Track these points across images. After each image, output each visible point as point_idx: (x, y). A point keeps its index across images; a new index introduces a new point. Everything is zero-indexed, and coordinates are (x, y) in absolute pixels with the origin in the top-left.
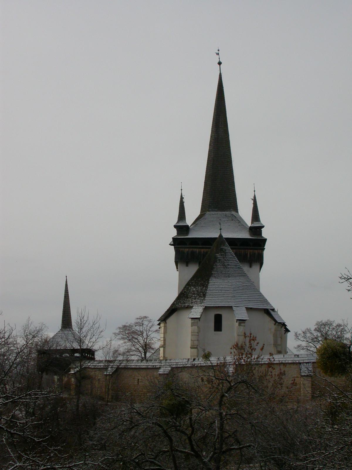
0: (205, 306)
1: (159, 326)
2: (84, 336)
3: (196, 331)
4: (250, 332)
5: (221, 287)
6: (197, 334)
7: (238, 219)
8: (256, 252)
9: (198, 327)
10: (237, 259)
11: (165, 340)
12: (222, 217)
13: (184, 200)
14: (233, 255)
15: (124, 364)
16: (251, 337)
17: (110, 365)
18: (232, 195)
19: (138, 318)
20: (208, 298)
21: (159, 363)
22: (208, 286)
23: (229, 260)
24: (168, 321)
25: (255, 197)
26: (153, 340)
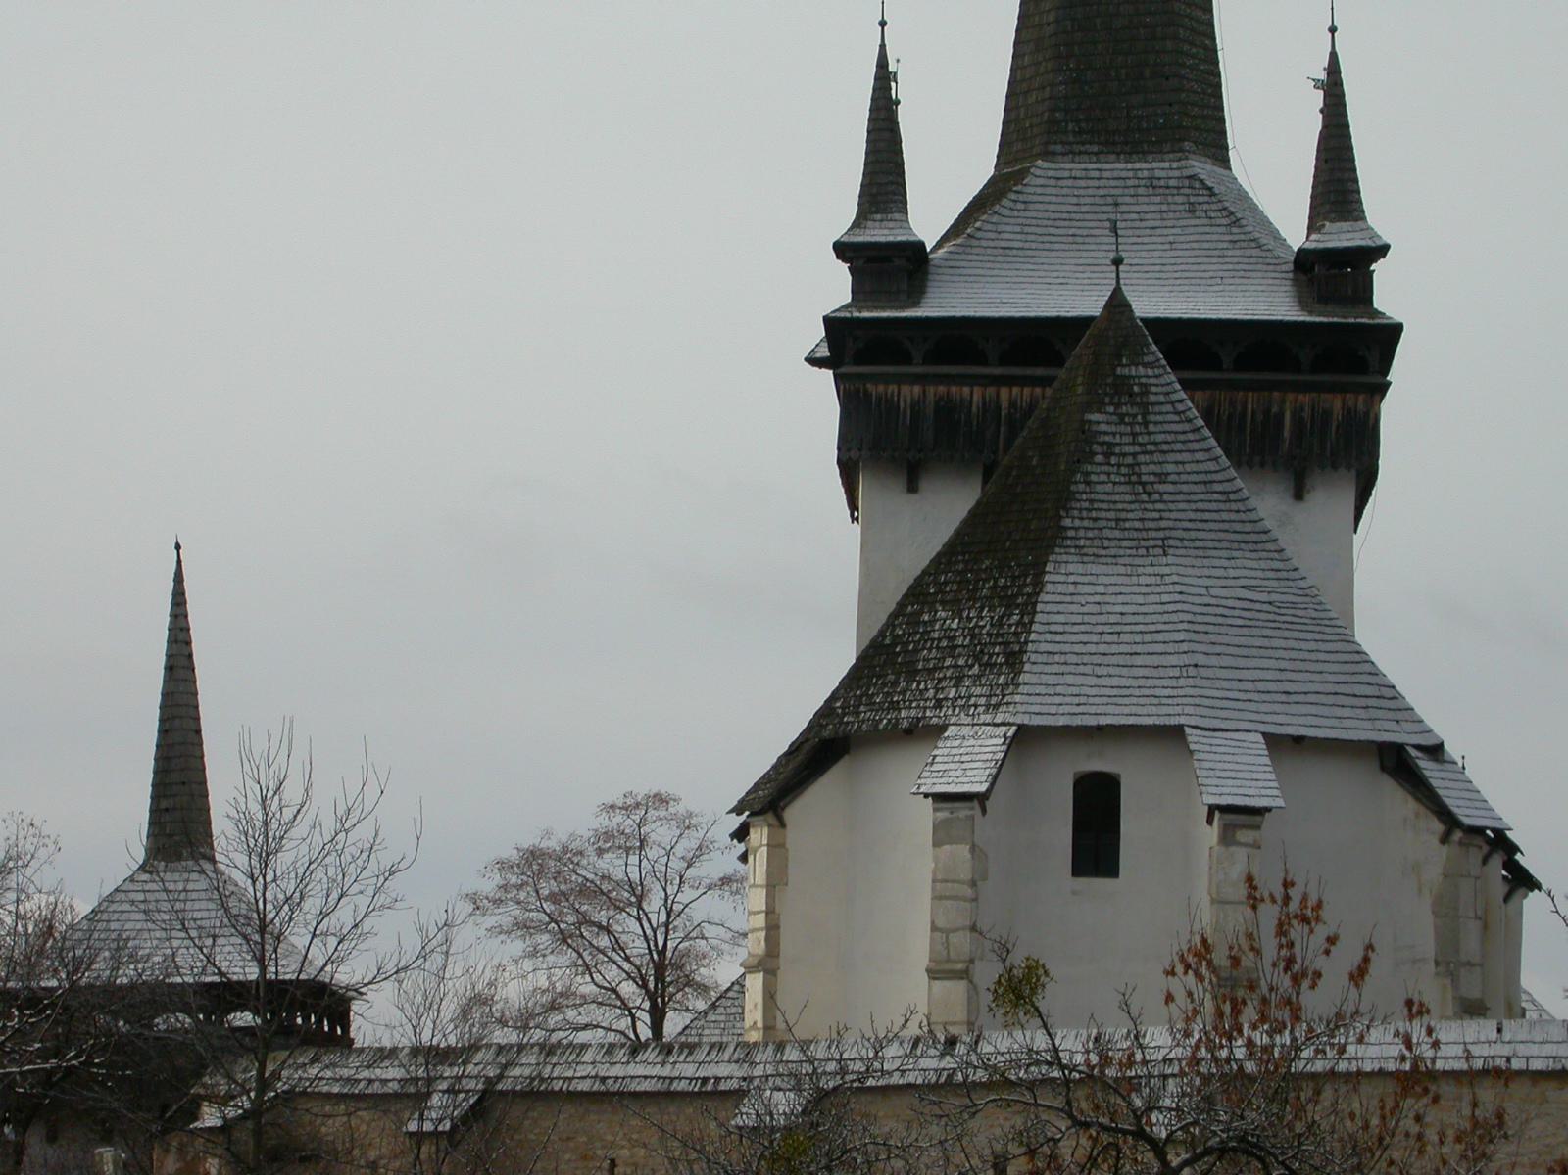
0: (1021, 727)
1: (741, 848)
2: (281, 897)
3: (965, 873)
4: (1286, 871)
5: (1119, 609)
6: (969, 892)
7: (1227, 204)
8: (1336, 404)
9: (973, 848)
10: (1213, 442)
11: (772, 929)
12: (1132, 191)
13: (901, 90)
14: (1189, 421)
15: (527, 1072)
16: (1287, 899)
17: (441, 1077)
18: (1193, 57)
19: (613, 807)
20: (1034, 679)
21: (737, 1062)
22: (1039, 607)
23: (1165, 447)
24: (796, 812)
25: (1333, 68)
26: (703, 938)
